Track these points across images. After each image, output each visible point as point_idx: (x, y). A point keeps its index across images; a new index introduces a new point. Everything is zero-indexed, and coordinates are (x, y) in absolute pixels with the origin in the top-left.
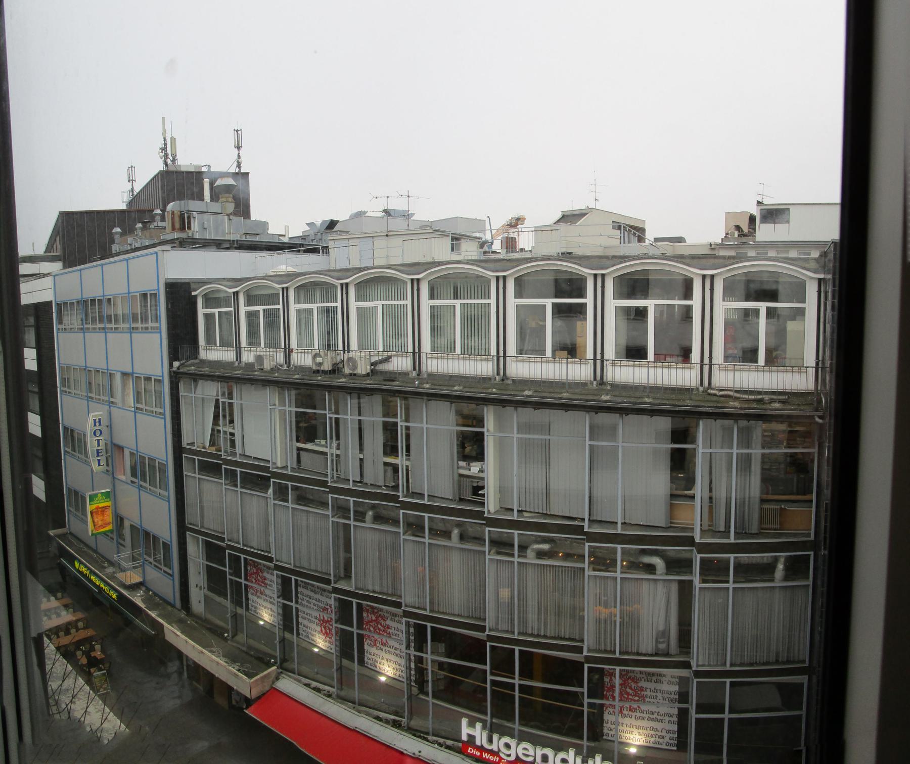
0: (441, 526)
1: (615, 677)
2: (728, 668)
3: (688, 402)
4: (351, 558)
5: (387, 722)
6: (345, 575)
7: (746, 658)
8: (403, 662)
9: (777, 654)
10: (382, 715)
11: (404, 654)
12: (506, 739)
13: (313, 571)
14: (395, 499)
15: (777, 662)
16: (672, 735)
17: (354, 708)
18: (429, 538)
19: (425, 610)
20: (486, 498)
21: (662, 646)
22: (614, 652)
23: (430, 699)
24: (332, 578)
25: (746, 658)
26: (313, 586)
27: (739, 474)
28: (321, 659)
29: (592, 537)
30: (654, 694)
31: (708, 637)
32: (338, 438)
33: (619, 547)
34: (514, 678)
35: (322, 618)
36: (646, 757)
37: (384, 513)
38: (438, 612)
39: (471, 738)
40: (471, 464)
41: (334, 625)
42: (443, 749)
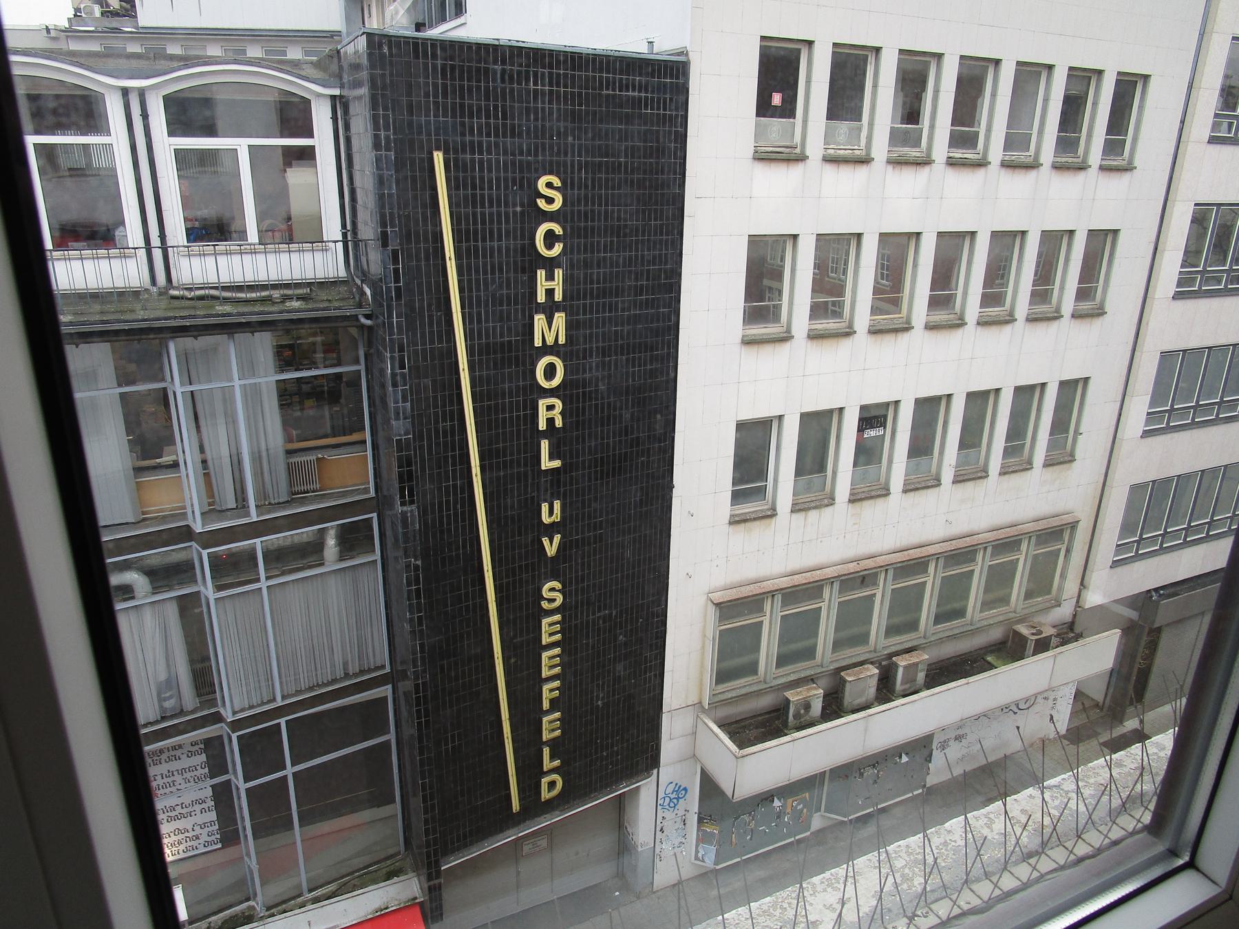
2: (280, 702)
3: (141, 314)
7: (302, 683)
9: (345, 664)
15: (347, 676)
16: (211, 829)
25: (302, 683)
30: (169, 780)
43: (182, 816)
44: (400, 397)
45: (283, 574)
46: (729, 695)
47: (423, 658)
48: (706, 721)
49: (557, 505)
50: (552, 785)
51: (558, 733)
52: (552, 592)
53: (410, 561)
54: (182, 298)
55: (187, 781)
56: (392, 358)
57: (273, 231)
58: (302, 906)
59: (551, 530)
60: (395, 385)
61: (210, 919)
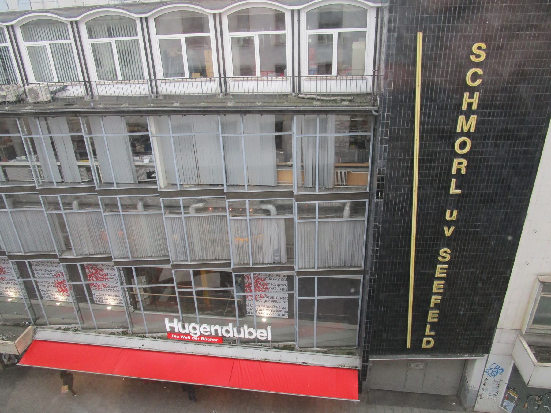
0: (129, 202)
1: (251, 279)
2: (316, 270)
4: (68, 236)
5: (118, 334)
6: (66, 248)
7: (326, 264)
8: (120, 294)
10: (114, 330)
11: (120, 289)
12: (193, 325)
13: (41, 252)
14: (92, 189)
15: (345, 266)
16: (285, 310)
17: (95, 332)
18: (123, 212)
19: (129, 258)
20: (157, 179)
21: (277, 258)
22: (249, 264)
23: (142, 312)
24: (57, 253)
25: (326, 264)
26: (44, 262)
27: (320, 149)
28: (64, 309)
29: (230, 196)
30: (274, 287)
31: (304, 251)
32: (35, 153)
33: (247, 200)
34: (192, 288)
35: (57, 282)
36: (272, 323)
37: (85, 200)
38: (138, 257)
39: (172, 328)
40: (143, 158)
41: (67, 283)
42: (156, 339)
43: (276, 302)
44: (383, 150)
45: (327, 217)
46: (540, 332)
47: (376, 268)
48: (522, 341)
49: (455, 212)
50: (428, 342)
51: (436, 320)
52: (445, 253)
53: (377, 224)
54: (303, 98)
55: (280, 289)
56: (382, 132)
57: (345, 70)
58: (312, 352)
59: (449, 224)
60: (381, 143)
61: (279, 343)
